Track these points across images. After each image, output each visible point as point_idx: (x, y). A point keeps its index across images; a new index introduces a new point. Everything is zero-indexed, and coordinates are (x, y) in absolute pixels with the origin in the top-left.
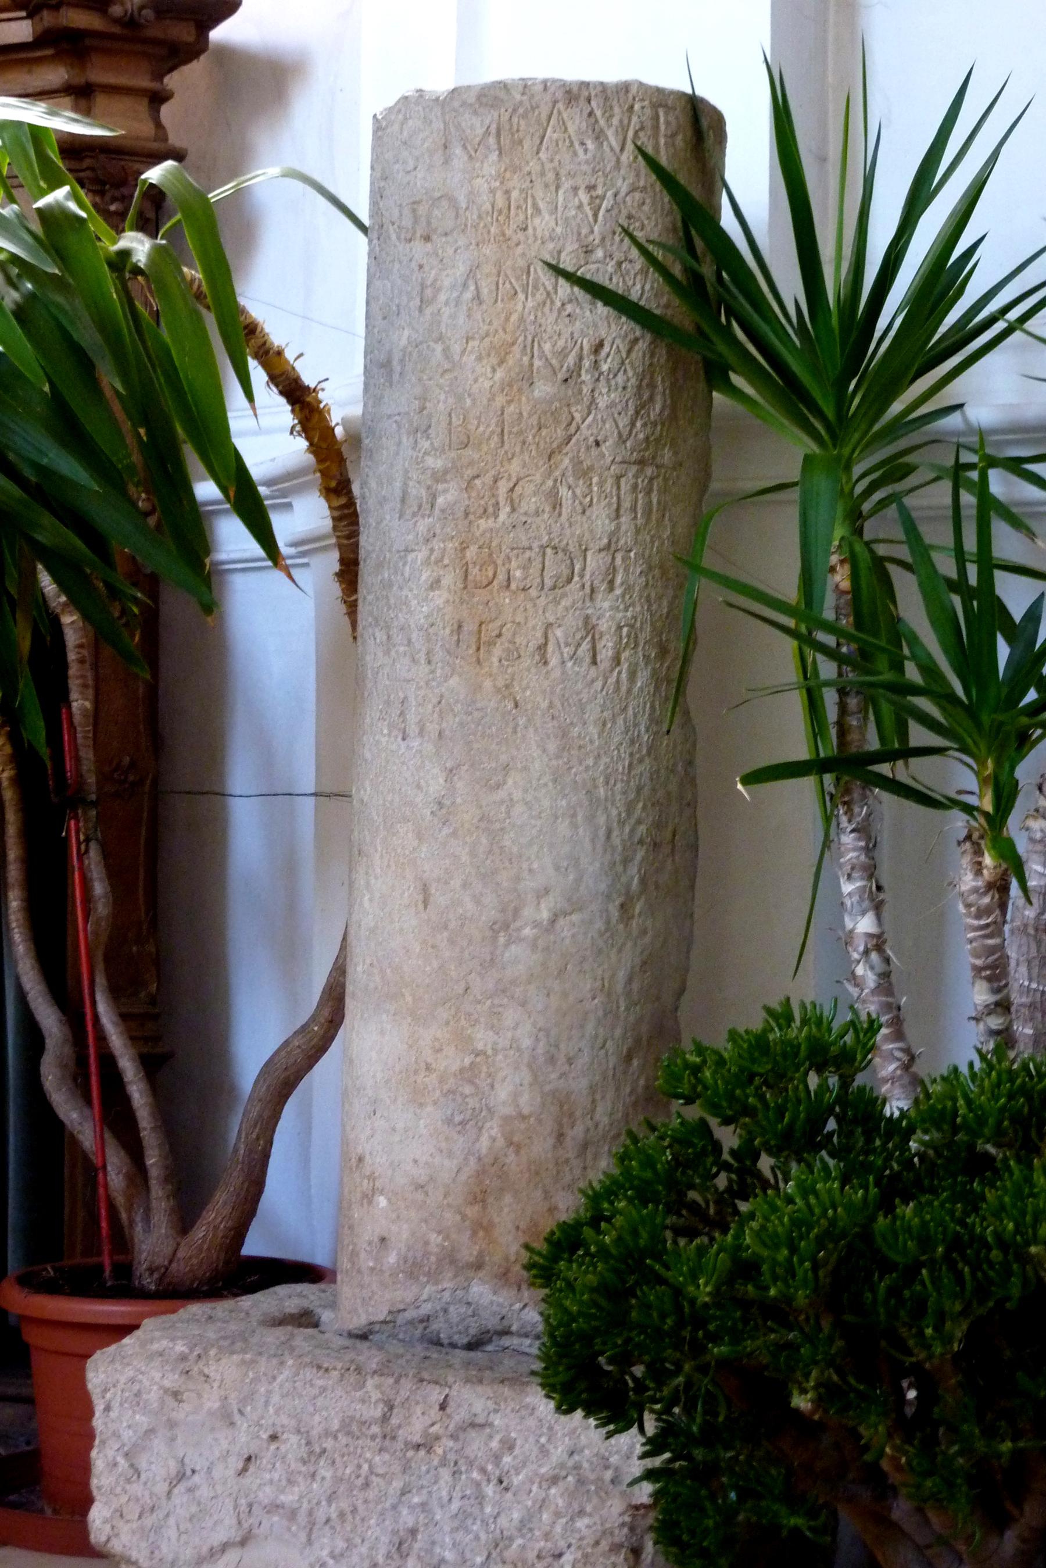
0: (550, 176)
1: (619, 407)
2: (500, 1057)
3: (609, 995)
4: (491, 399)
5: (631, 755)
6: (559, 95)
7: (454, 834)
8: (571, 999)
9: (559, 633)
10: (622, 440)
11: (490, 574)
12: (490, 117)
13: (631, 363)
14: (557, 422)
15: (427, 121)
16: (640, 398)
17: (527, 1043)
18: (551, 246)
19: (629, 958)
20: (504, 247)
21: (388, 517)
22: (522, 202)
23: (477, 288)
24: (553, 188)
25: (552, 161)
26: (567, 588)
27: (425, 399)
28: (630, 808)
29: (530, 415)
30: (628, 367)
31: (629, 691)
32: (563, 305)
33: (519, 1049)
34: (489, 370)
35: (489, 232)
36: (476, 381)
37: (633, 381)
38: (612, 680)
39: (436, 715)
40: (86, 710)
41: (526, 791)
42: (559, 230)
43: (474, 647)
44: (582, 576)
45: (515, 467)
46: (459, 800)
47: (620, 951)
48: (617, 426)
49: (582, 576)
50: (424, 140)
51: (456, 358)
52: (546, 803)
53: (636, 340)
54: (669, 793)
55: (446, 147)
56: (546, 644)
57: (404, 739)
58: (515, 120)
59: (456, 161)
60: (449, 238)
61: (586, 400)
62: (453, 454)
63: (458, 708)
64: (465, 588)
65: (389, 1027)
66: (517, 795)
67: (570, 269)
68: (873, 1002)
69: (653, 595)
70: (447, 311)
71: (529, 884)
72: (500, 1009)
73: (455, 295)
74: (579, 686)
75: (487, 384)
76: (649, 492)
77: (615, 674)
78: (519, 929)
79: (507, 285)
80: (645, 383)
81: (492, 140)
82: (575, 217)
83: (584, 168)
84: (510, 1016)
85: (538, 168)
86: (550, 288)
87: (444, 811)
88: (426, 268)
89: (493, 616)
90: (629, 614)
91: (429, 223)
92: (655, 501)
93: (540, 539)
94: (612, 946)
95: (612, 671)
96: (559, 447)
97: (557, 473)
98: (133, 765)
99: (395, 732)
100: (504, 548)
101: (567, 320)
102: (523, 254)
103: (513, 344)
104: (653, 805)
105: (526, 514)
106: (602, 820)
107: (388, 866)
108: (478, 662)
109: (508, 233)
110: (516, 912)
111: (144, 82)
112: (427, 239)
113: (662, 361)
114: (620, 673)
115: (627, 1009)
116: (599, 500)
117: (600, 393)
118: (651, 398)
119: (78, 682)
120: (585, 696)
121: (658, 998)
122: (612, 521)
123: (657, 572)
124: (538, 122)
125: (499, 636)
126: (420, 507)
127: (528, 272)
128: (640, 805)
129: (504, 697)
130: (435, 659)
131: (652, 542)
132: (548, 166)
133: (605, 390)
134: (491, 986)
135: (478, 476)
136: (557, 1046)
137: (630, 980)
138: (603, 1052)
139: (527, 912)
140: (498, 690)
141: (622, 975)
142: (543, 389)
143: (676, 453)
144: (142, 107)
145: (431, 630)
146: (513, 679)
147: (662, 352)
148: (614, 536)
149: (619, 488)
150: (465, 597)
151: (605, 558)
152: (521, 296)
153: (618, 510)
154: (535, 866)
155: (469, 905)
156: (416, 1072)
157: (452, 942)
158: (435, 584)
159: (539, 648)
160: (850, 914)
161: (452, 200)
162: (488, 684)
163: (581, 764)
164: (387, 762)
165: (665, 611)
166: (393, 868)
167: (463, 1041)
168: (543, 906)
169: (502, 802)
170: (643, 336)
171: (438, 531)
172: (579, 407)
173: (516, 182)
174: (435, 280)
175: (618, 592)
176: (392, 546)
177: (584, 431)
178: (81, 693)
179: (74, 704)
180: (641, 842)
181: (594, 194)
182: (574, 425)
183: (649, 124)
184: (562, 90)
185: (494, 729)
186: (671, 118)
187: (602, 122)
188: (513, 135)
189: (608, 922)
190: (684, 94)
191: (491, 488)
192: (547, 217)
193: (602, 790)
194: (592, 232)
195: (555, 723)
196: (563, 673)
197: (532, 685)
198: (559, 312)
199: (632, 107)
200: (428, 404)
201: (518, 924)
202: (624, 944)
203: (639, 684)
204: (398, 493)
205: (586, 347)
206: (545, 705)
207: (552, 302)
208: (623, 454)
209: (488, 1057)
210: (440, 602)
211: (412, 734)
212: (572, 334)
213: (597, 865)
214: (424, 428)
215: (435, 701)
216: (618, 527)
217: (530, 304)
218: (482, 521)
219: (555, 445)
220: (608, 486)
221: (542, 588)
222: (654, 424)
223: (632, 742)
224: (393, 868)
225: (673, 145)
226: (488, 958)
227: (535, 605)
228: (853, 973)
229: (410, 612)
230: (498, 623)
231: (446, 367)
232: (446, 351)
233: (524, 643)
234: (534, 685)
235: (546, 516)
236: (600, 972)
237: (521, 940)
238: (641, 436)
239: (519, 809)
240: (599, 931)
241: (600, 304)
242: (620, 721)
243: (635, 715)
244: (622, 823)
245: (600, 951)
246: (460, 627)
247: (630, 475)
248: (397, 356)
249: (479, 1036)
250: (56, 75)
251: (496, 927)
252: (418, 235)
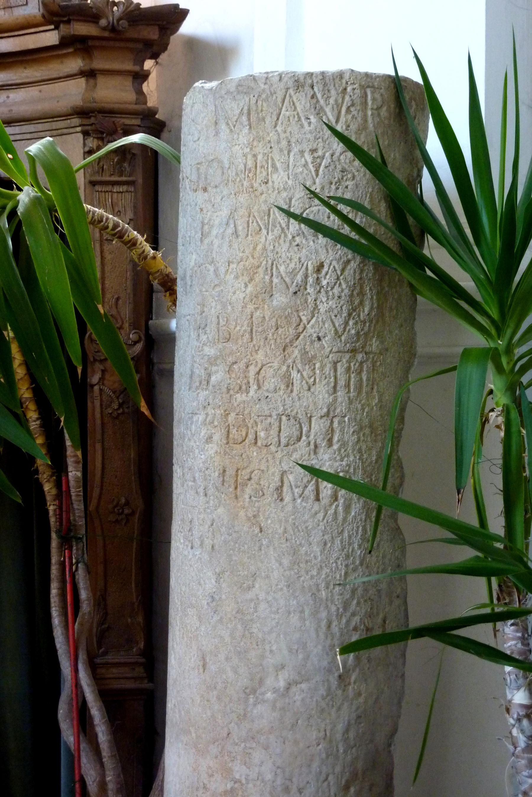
0: (284, 143)
1: (336, 312)
2: (251, 785)
3: (331, 741)
4: (244, 307)
5: (347, 566)
6: (290, 84)
7: (221, 620)
8: (301, 745)
9: (291, 477)
10: (337, 335)
11: (244, 434)
12: (244, 101)
13: (345, 279)
14: (289, 323)
15: (205, 105)
16: (352, 302)
17: (269, 777)
18: (284, 194)
19: (347, 713)
20: (253, 196)
21: (183, 388)
22: (264, 163)
23: (235, 226)
24: (286, 152)
25: (285, 132)
26: (297, 445)
27: (204, 305)
28: (346, 605)
29: (270, 319)
30: (342, 281)
31: (345, 519)
32: (293, 237)
33: (263, 781)
34: (243, 285)
35: (242, 185)
36: (234, 293)
37: (346, 291)
38: (331, 511)
39: (210, 534)
40: (77, 478)
41: (268, 593)
42: (290, 182)
43: (233, 487)
44: (308, 437)
45: (260, 357)
46: (224, 597)
47: (339, 709)
48: (334, 326)
49: (308, 437)
50: (204, 118)
51: (222, 276)
52: (282, 602)
53: (349, 261)
54: (379, 591)
55: (216, 123)
56: (282, 486)
57: (192, 548)
58: (260, 103)
59: (222, 134)
60: (218, 189)
61: (311, 306)
62: (220, 346)
63: (223, 529)
64: (228, 443)
65: (183, 752)
66: (262, 596)
67: (298, 212)
68: (523, 758)
69: (364, 447)
70: (216, 242)
71: (270, 661)
72: (251, 751)
73: (222, 230)
74: (306, 517)
75: (242, 296)
76: (359, 372)
77: (334, 507)
78: (263, 694)
79: (255, 224)
80: (357, 292)
81: (244, 118)
82: (302, 173)
83: (309, 136)
84: (258, 756)
85: (275, 137)
86: (284, 225)
87: (214, 603)
88: (205, 211)
89: (245, 465)
90: (344, 463)
91: (206, 178)
92: (364, 378)
93: (276, 409)
94: (333, 706)
95: (331, 505)
96: (291, 342)
97: (290, 361)
98: (127, 503)
99: (187, 543)
100: (253, 415)
101: (296, 248)
102: (266, 201)
103: (258, 267)
104: (365, 601)
105: (267, 391)
106: (324, 614)
107: (183, 638)
108: (236, 497)
109: (256, 185)
110: (261, 682)
111: (129, 66)
112: (205, 190)
113: (370, 275)
114: (337, 506)
115: (345, 752)
116: (320, 380)
117: (321, 301)
118: (361, 303)
119: (72, 459)
120: (310, 525)
121: (372, 741)
122: (330, 395)
123: (367, 431)
124: (275, 104)
125: (250, 479)
126: (200, 383)
127: (269, 215)
128: (355, 602)
129: (254, 524)
130: (210, 492)
131: (363, 409)
132: (283, 136)
133: (324, 299)
134: (244, 733)
135: (236, 363)
136: (290, 780)
137: (347, 731)
138: (326, 783)
139: (269, 682)
140: (249, 519)
141: (340, 727)
142: (280, 299)
143: (382, 342)
144: (128, 82)
145: (207, 472)
146: (259, 511)
147: (370, 268)
148: (331, 407)
149: (336, 371)
150: (227, 450)
151: (325, 423)
152: (264, 231)
153: (335, 387)
154: (274, 648)
155: (230, 674)
156: (197, 789)
157: (219, 698)
158: (209, 439)
159: (277, 489)
160: (509, 688)
161: (220, 162)
162: (242, 513)
163: (307, 574)
164: (182, 563)
165: (374, 458)
166: (185, 639)
167: (227, 772)
168: (280, 677)
169: (251, 600)
170: (354, 258)
171: (211, 402)
172: (305, 312)
173: (260, 149)
174: (210, 220)
175: (335, 447)
176: (184, 410)
177: (310, 330)
178: (75, 467)
179: (70, 474)
180: (355, 629)
181: (316, 155)
182: (302, 325)
183: (358, 101)
184: (293, 80)
185: (246, 546)
186: (378, 96)
187: (322, 102)
188: (258, 114)
189: (329, 689)
190: (390, 76)
191: (245, 372)
192: (282, 173)
193: (323, 593)
194: (315, 183)
195: (288, 544)
196: (294, 507)
197: (272, 515)
198: (291, 244)
199: (345, 89)
200: (205, 309)
201: (263, 689)
202: (342, 704)
203: (353, 514)
204: (189, 372)
205: (310, 268)
206: (281, 531)
207: (286, 236)
208: (339, 345)
209: (242, 785)
210: (212, 452)
211: (196, 546)
212: (300, 258)
213: (320, 647)
214: (202, 326)
215: (209, 523)
216: (335, 400)
217: (270, 237)
218: (238, 395)
219: (288, 340)
220: (328, 369)
221: (279, 445)
222: (364, 322)
223: (347, 557)
224: (185, 639)
225: (379, 115)
226: (242, 714)
227: (274, 458)
228: (511, 733)
229: (194, 458)
230: (248, 470)
231: (216, 283)
232: (216, 271)
233: (267, 485)
234: (273, 516)
235: (281, 392)
236: (323, 726)
237: (264, 701)
238: (353, 332)
239: (263, 606)
240: (323, 696)
241: (320, 236)
242: (338, 542)
243: (350, 537)
244: (339, 617)
245: (323, 711)
246: (224, 471)
247: (344, 360)
248: (189, 273)
249: (236, 769)
250: (75, 64)
251: (247, 691)
252: (200, 187)
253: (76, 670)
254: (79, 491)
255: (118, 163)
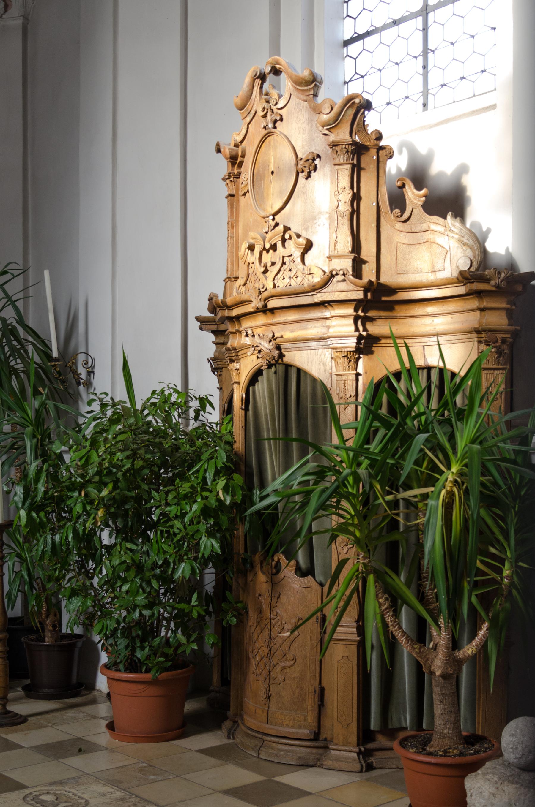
253: (442, 437)
254: (449, 644)
255: (497, 358)
